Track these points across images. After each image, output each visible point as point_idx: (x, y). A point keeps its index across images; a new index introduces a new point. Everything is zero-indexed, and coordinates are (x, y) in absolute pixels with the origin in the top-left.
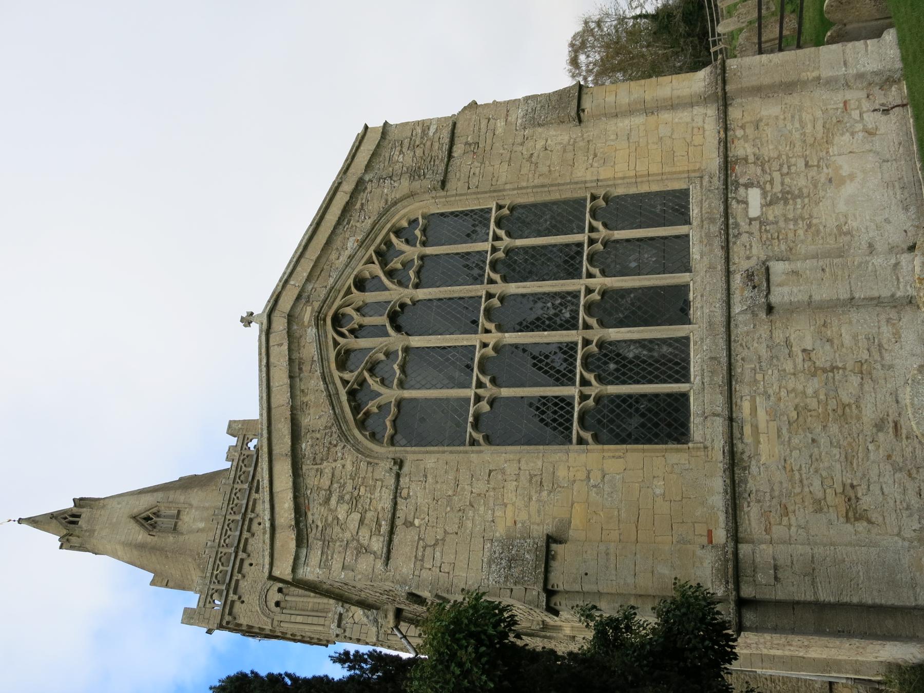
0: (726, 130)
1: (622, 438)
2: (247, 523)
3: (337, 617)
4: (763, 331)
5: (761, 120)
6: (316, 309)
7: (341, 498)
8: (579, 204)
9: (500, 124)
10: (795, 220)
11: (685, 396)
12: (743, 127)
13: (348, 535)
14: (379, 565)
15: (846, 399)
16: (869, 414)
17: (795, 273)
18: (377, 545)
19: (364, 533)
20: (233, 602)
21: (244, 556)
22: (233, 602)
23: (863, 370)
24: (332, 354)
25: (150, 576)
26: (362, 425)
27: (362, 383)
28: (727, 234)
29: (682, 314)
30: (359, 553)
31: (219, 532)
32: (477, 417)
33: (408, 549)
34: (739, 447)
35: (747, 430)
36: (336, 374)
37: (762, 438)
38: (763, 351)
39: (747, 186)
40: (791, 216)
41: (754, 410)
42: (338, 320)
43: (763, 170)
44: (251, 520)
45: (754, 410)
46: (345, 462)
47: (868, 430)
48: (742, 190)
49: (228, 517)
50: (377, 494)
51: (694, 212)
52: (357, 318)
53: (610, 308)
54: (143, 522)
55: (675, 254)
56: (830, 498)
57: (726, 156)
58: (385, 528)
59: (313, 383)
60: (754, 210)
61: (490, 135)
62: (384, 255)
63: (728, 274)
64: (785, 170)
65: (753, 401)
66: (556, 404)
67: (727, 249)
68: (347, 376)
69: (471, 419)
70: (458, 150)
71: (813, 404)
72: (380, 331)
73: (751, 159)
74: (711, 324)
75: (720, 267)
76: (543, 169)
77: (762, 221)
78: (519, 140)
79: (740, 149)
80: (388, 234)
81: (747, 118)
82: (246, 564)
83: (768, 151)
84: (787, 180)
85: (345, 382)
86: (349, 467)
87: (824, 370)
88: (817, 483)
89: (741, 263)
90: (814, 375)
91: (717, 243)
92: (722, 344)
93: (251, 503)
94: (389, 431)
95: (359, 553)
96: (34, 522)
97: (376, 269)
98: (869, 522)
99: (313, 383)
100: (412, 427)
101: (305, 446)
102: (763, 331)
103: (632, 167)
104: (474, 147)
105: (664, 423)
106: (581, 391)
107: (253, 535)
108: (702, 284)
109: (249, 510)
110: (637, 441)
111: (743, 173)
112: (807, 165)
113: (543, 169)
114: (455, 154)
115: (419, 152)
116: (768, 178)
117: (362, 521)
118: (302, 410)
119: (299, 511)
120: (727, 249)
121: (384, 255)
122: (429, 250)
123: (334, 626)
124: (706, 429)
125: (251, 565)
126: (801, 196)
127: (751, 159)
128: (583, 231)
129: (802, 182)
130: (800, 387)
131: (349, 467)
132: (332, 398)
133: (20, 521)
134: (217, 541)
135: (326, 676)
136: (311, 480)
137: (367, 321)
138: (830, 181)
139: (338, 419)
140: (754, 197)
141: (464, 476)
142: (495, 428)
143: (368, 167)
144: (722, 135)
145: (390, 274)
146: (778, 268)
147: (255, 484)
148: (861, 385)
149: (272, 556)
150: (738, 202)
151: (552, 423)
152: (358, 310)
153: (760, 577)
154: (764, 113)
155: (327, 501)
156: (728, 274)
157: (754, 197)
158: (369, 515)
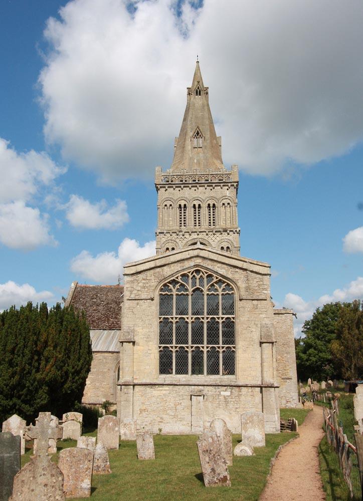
0: (251, 387)
1: (161, 357)
3: (162, 231)
5: (254, 396)
7: (144, 283)
8: (233, 342)
9: (264, 316)
10: (219, 404)
11: (187, 373)
12: (252, 391)
13: (135, 287)
14: (127, 298)
15: (168, 412)
16: (164, 416)
17: (199, 403)
18: (133, 296)
22: (165, 187)
23: (175, 416)
24: (185, 272)
26: (165, 285)
28: (216, 386)
29: (179, 372)
30: (130, 291)
31: (190, 174)
32: (168, 318)
33: (131, 305)
34: (157, 386)
35: (161, 388)
36: (180, 274)
37: (159, 392)
38: (181, 393)
39: (231, 392)
40: (220, 403)
41: (165, 390)
42: (198, 271)
43: (236, 396)
45: (165, 390)
46: (154, 283)
47: (161, 416)
48: (230, 390)
49: (197, 176)
50: (145, 293)
52: (198, 277)
54: (196, 132)
55: (214, 370)
56: (145, 406)
57: (242, 386)
58: (137, 298)
59: (177, 267)
60: (222, 393)
61: (260, 312)
62: (220, 282)
63: (204, 385)
64: (235, 402)
65: (168, 390)
66: (217, 328)
68: (180, 278)
69: (166, 317)
71: (168, 404)
72: (194, 284)
73: (240, 393)
74: (189, 380)
75: (206, 384)
77: (219, 395)
78: (256, 323)
79: (244, 389)
80: (226, 282)
81: (255, 393)
83: (242, 398)
84: (232, 402)
85: (177, 278)
86: (153, 284)
87: (176, 407)
88: (148, 403)
90: (175, 405)
91: (214, 383)
92: (183, 383)
94: (164, 293)
95: (130, 291)
96: (198, 68)
97: (215, 280)
98: (140, 414)
99: (177, 267)
100: (165, 300)
101: (158, 269)
102: (186, 394)
103: (242, 359)
105: (165, 368)
106: (174, 347)
108: (213, 378)
110: (160, 361)
111: (236, 390)
112: (237, 408)
114: (253, 301)
115: (257, 288)
116: (233, 397)
117: (138, 290)
119: (140, 272)
121: (220, 282)
122: (220, 297)
123: (159, 231)
125: (179, 191)
126: (226, 405)
127: (240, 393)
128: (223, 344)
129: (231, 406)
130: (171, 401)
131: (153, 284)
132: (172, 275)
134: (187, 174)
136: (148, 273)
137: (198, 281)
138: (231, 414)
139: (165, 279)
141: (150, 317)
142: (165, 324)
143: (252, 271)
144: (249, 385)
148: (171, 415)
149: (129, 267)
150: (226, 389)
151: (164, 338)
152: (201, 276)
153: (125, 390)
154: (256, 398)
155: (144, 280)
156: (204, 385)
157: (228, 393)
158: (140, 292)
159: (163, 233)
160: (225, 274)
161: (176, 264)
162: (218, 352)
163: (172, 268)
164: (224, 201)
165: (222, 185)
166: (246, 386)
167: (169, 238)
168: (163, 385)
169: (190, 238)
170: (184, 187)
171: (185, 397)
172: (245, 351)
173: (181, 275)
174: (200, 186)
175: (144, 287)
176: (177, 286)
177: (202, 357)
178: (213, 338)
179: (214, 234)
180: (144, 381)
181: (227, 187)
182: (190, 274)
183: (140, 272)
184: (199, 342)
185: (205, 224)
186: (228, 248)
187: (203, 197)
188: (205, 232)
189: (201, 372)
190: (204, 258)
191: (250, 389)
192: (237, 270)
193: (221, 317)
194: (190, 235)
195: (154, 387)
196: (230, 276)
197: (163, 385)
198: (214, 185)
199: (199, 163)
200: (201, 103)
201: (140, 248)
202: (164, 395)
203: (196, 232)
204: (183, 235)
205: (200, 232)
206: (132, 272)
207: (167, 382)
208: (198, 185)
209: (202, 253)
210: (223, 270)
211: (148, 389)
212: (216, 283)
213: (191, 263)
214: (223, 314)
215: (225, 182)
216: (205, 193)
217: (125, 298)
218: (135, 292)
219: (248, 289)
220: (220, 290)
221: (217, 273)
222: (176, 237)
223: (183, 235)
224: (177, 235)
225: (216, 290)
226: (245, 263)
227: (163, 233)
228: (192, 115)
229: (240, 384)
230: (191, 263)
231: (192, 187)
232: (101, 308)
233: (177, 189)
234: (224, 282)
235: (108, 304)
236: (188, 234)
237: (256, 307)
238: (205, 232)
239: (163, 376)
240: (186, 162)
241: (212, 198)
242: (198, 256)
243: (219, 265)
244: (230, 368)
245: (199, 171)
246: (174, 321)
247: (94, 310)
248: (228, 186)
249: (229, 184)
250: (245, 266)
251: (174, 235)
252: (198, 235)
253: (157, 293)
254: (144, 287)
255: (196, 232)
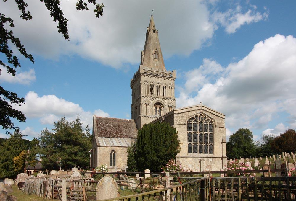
4: (198, 160)
9: (223, 133)
11: (192, 153)
14: (176, 123)
18: (178, 123)
19: (178, 121)
22: (144, 75)
24: (197, 115)
25: (8, 139)
26: (189, 119)
27: (194, 119)
31: (156, 71)
36: (195, 116)
51: (210, 154)
52: (201, 117)
53: (206, 146)
55: (206, 152)
58: (179, 123)
59: (194, 113)
63: (204, 157)
67: (206, 157)
70: (220, 128)
76: (217, 138)
83: (216, 162)
89: (204, 158)
91: (207, 157)
99: (194, 113)
102: (198, 160)
104: (220, 130)
105: (190, 151)
106: (193, 143)
108: (206, 155)
113: (217, 138)
117: (180, 121)
118: (69, 135)
119: (180, 113)
120: (206, 157)
121: (209, 120)
122: (208, 125)
124: (190, 155)
132: (192, 116)
140: (211, 160)
143: (219, 117)
145: (206, 121)
146: (204, 162)
155: (182, 116)
156: (204, 157)
157: (211, 160)
159: (144, 96)
160: (211, 117)
161: (193, 111)
162: (208, 145)
163: (192, 113)
164: (170, 86)
165: (169, 78)
166: (217, 158)
167: (147, 99)
168: (190, 157)
169: (155, 100)
170: (153, 76)
171: (197, 161)
172: (217, 145)
173: (196, 116)
174: (160, 77)
175: (182, 119)
176: (194, 120)
177: (192, 147)
178: (206, 140)
179: (166, 100)
180: (183, 156)
181: (171, 80)
182: (198, 116)
183: (180, 113)
184: (202, 141)
185: (162, 96)
186: (171, 106)
187: (168, 83)
188: (162, 98)
189: (197, 153)
190: (204, 110)
191: (218, 159)
192: (215, 116)
193: (209, 133)
194: (156, 99)
195: (187, 158)
196: (212, 118)
197: (190, 157)
198: (166, 78)
199: (157, 66)
200: (155, 37)
201: (39, 98)
202: (190, 161)
203: (158, 98)
204: (153, 99)
205: (160, 98)
206: (177, 113)
207: (191, 156)
208: (159, 77)
209: (203, 108)
210: (210, 115)
211: (185, 159)
212: (207, 120)
213: (199, 111)
214: (209, 132)
215: (147, 74)
216: (162, 81)
217: (175, 123)
218: (178, 121)
219: (218, 123)
220: (209, 123)
221: (208, 116)
222: (150, 99)
223: (153, 99)
224: (150, 98)
225: (191, 122)
226: (217, 113)
227: (144, 96)
228: (152, 42)
229: (215, 157)
230: (199, 111)
231: (156, 77)
232: (112, 128)
233: (157, 78)
234: (210, 120)
235: (114, 126)
236: (155, 98)
237: (220, 130)
238: (162, 98)
239: (189, 154)
240: (152, 64)
241: (165, 83)
242: (202, 109)
243: (209, 113)
244: (211, 152)
245: (155, 69)
246: (193, 133)
247: (109, 129)
248: (171, 79)
249: (172, 79)
250: (217, 114)
251: (149, 98)
252: (159, 99)
253: (187, 122)
254: (182, 119)
255: (158, 98)
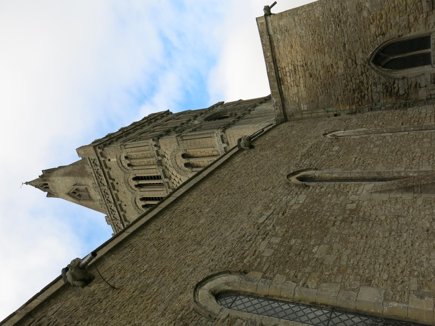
2: (118, 207)
6: (169, 213)
20: (104, 161)
21: (116, 192)
44: (120, 205)
54: (73, 195)
59: (205, 126)
82: (107, 162)
93: (115, 196)
107: (125, 212)
109: (116, 200)
133: (27, 183)
135: (222, 103)
147: (111, 186)
